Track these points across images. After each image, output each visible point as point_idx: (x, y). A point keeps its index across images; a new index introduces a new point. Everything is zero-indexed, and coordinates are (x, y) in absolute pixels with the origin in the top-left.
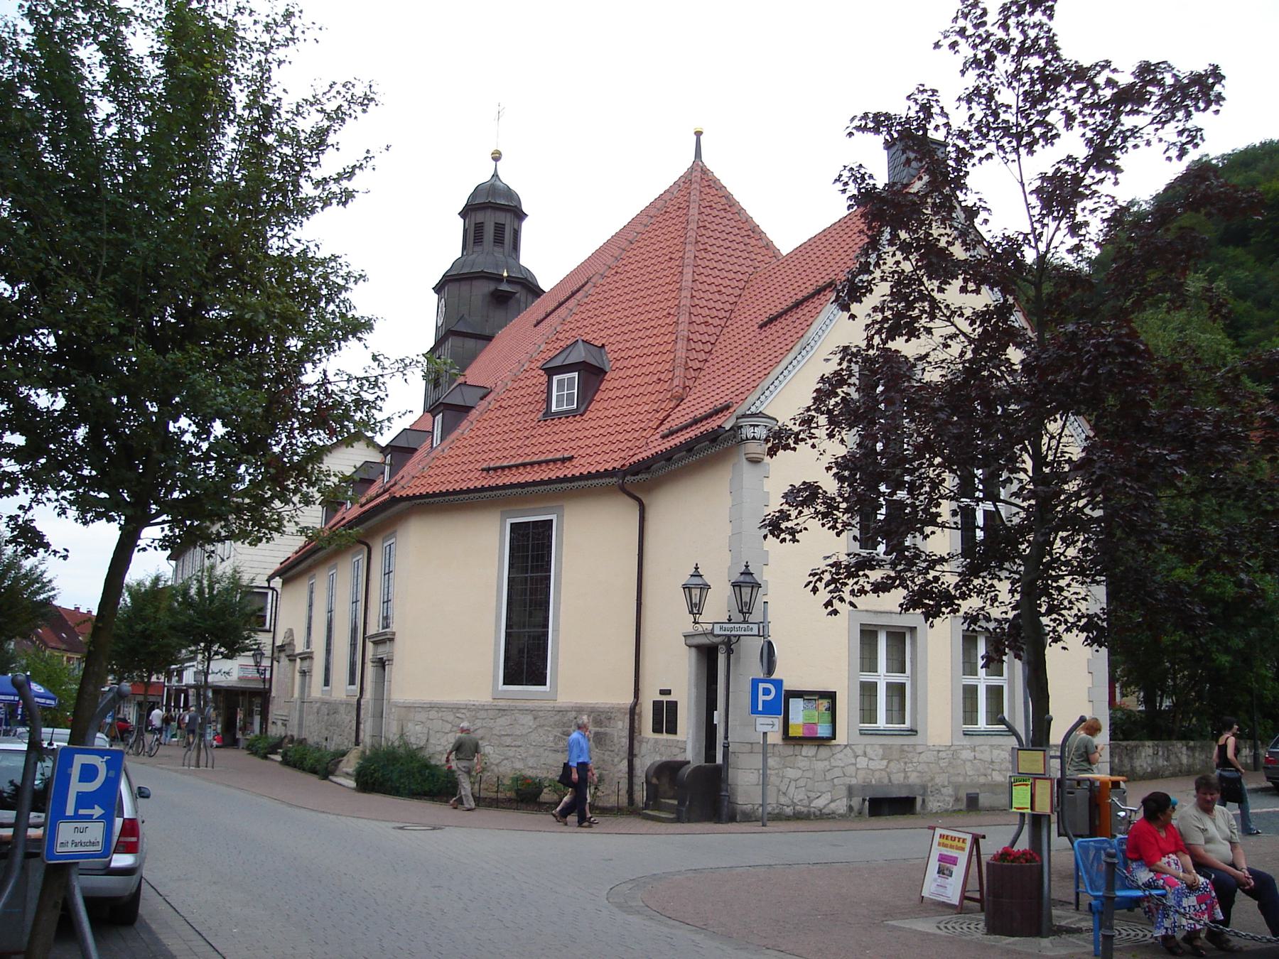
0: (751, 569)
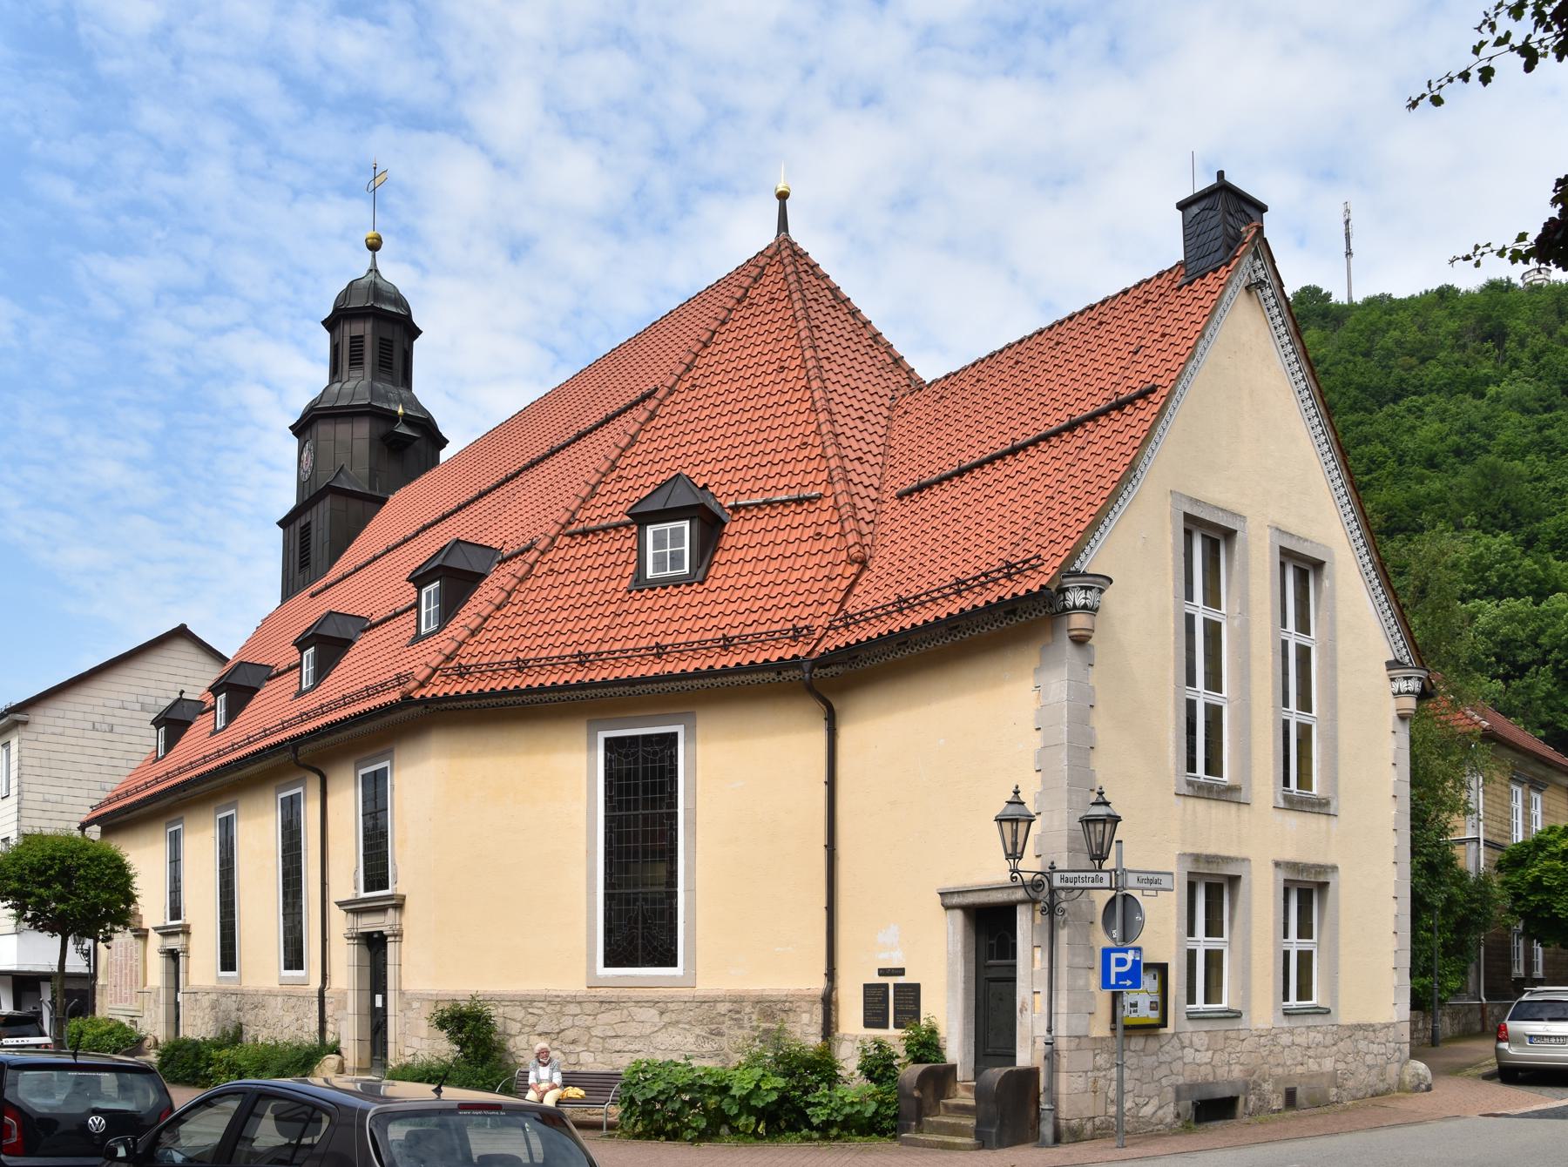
0: (1107, 797)
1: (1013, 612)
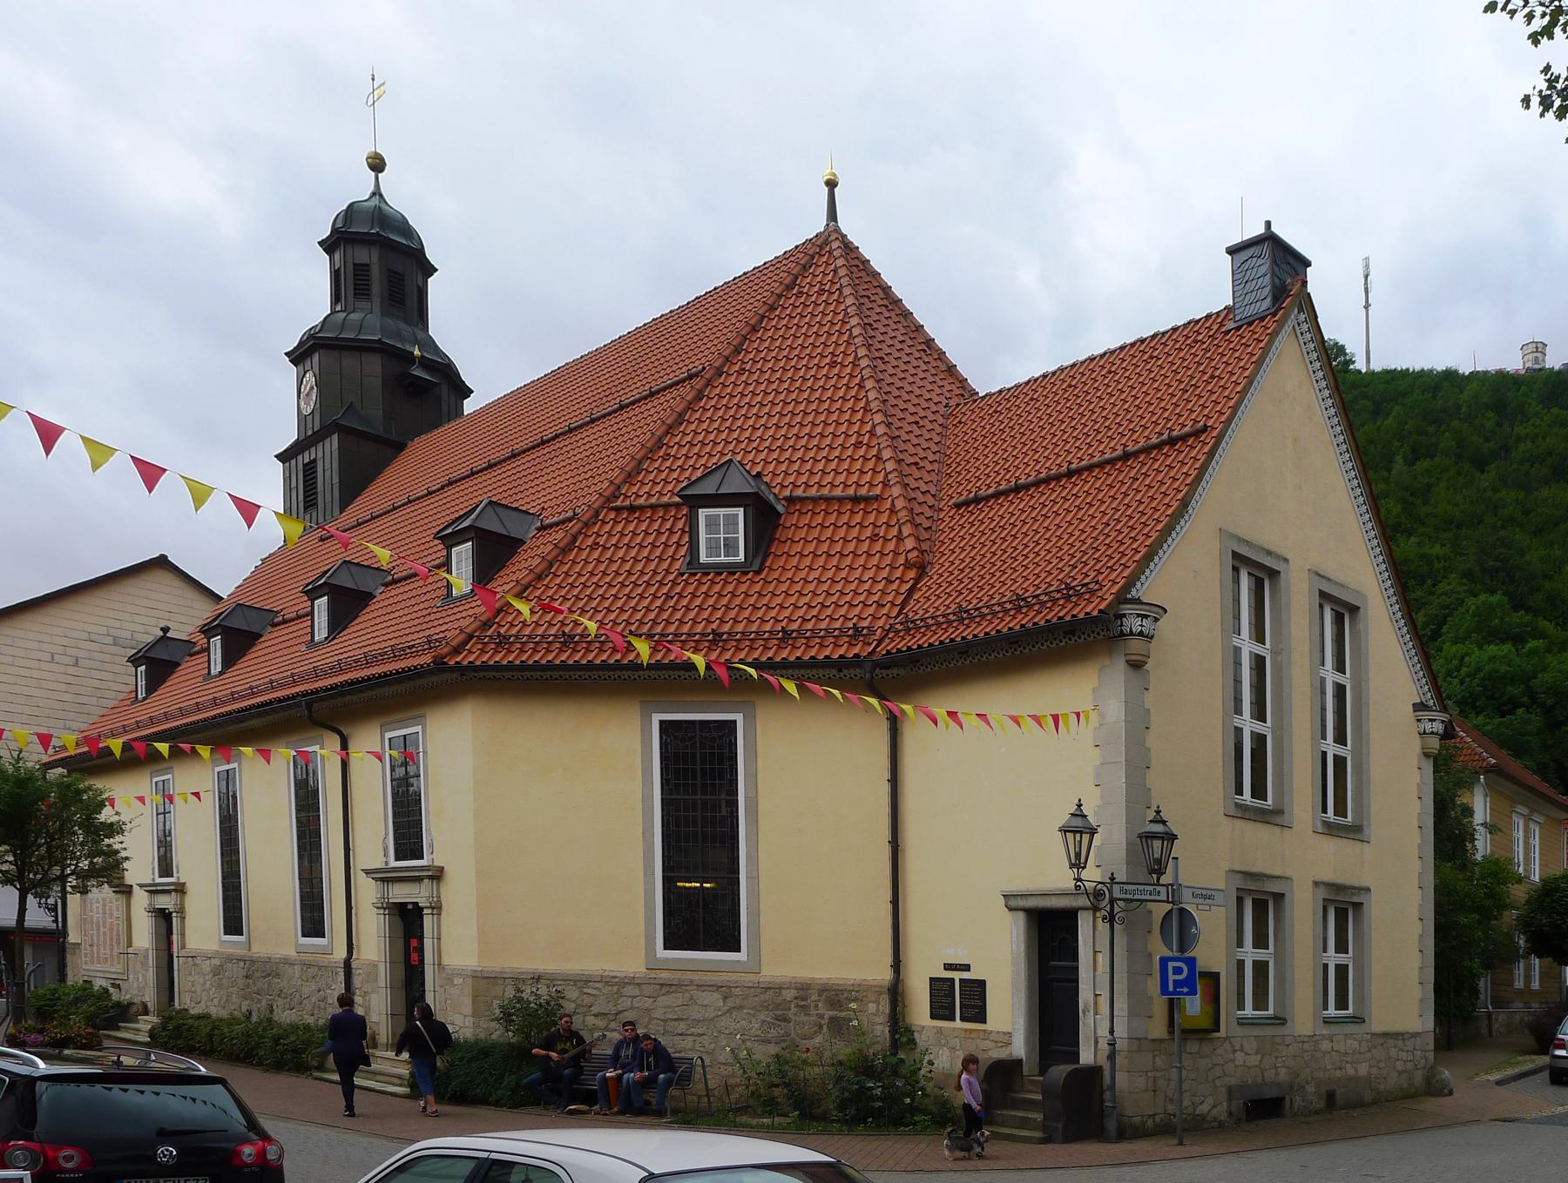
1: (1073, 632)
